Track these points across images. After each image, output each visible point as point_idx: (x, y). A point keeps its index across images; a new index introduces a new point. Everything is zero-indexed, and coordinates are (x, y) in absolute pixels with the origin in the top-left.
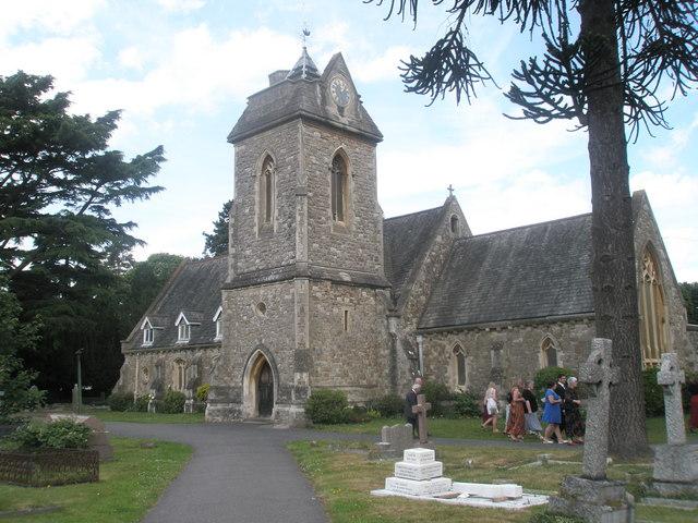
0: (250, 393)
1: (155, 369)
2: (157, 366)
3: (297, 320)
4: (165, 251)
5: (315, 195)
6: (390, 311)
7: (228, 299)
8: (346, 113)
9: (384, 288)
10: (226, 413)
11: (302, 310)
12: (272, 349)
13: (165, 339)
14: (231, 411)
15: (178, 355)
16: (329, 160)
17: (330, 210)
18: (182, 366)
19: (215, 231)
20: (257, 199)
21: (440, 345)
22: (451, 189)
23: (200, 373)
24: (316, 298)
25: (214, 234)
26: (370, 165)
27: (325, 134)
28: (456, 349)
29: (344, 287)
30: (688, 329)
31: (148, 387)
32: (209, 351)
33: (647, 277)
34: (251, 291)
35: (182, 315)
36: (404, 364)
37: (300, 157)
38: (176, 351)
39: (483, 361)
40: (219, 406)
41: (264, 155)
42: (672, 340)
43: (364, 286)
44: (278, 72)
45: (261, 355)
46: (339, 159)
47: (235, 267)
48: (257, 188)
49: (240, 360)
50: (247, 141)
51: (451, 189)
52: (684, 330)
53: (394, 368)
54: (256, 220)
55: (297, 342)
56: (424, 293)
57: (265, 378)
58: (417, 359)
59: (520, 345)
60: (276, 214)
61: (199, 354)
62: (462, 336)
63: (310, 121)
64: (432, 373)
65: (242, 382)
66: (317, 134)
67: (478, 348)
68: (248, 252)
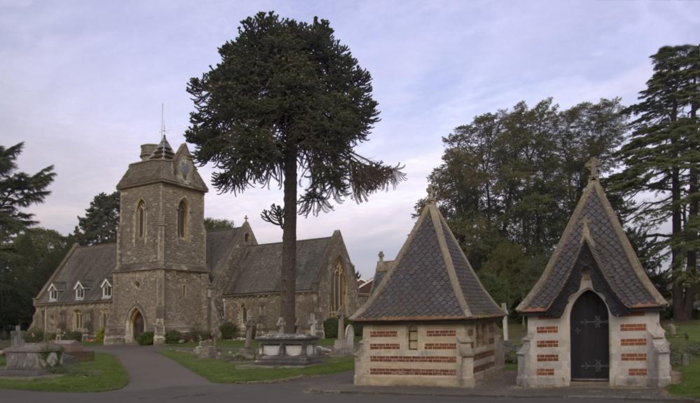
0: (130, 329)
1: (59, 316)
2: (61, 314)
3: (158, 291)
4: (56, 230)
5: (169, 225)
6: (208, 285)
7: (117, 278)
8: (187, 178)
9: (205, 273)
10: (115, 340)
11: (161, 286)
12: (143, 306)
13: (65, 297)
14: (119, 339)
15: (76, 307)
16: (177, 205)
17: (177, 233)
18: (79, 314)
19: (87, 215)
20: (134, 223)
21: (234, 304)
22: (246, 218)
23: (92, 318)
24: (168, 280)
25: (86, 217)
26: (200, 206)
27: (175, 191)
28: (243, 305)
29: (184, 274)
30: (359, 296)
31: (54, 327)
32: (98, 306)
33: (337, 272)
34: (131, 275)
35: (78, 283)
36: (214, 313)
37: (161, 204)
38: (74, 305)
39: (255, 312)
40: (112, 337)
41: (139, 200)
42: (349, 301)
43: (194, 272)
44: (148, 145)
45: (136, 309)
46: (183, 203)
47: (120, 260)
48: (134, 217)
49: (124, 312)
50: (129, 190)
51: (246, 218)
52: (357, 296)
53: (209, 315)
54: (134, 236)
55: (158, 302)
56: (228, 276)
57: (693, 268)
58: (222, 311)
59: (274, 304)
60: (146, 233)
61: (91, 307)
62: (246, 299)
63: (166, 184)
64: (230, 317)
65: (125, 323)
66: (171, 191)
67: (253, 305)
68: (129, 253)
